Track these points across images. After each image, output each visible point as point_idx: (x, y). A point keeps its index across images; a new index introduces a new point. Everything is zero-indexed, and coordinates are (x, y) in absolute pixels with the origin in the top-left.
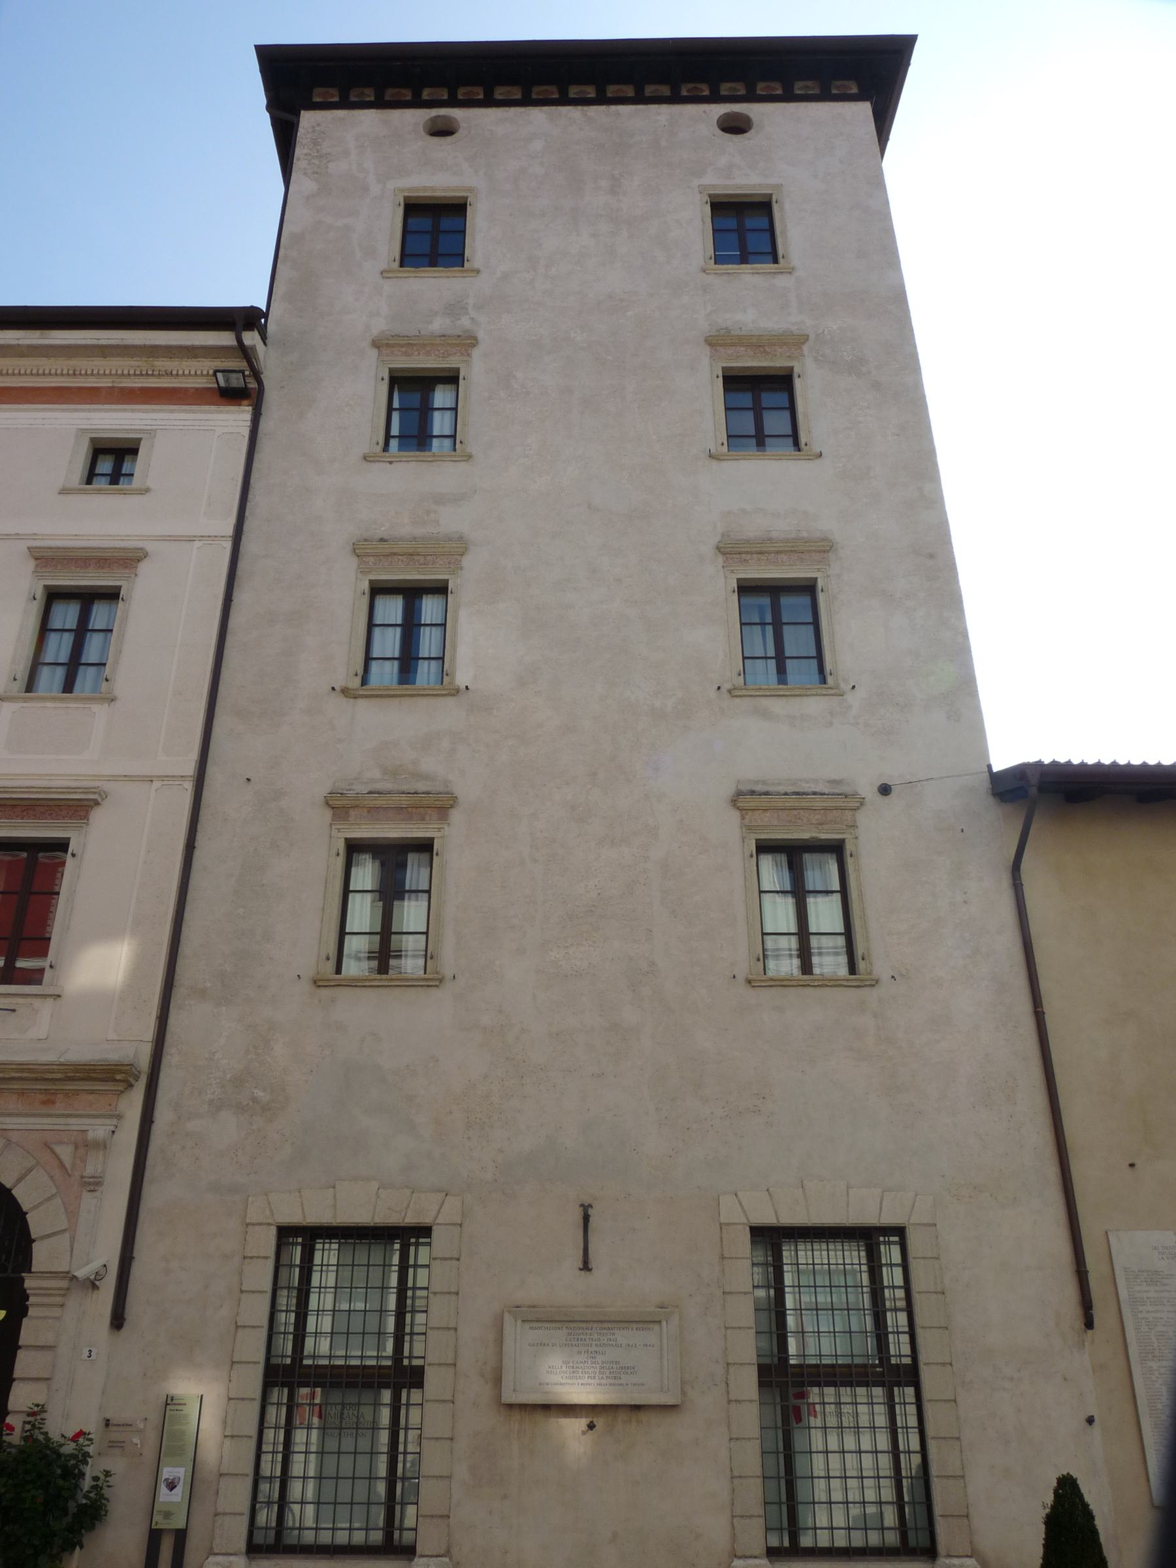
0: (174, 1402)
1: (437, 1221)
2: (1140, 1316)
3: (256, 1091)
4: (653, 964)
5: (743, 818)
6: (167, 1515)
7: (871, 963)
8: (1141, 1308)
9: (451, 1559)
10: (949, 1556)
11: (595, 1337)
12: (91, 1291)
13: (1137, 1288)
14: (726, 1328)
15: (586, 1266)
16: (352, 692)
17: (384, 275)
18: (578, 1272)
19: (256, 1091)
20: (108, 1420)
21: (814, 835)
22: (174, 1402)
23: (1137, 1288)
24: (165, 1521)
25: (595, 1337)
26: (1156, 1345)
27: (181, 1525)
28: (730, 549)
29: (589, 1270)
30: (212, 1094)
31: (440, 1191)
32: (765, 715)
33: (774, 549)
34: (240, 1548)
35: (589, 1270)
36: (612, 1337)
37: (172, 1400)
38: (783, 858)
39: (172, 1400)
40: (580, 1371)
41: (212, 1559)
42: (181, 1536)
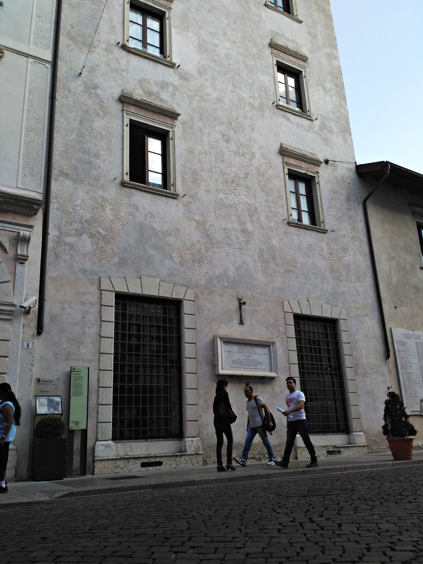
0: (75, 370)
1: (185, 298)
2: (400, 355)
3: (99, 229)
4: (256, 208)
5: (283, 159)
6: (77, 423)
7: (325, 225)
8: (401, 353)
9: (199, 438)
10: (356, 432)
11: (248, 350)
12: (23, 315)
13: (399, 346)
14: (98, 405)
15: (241, 323)
16: (128, 48)
17: (149, 215)
18: (239, 325)
19: (99, 229)
20: (39, 379)
21: (306, 172)
22: (75, 370)
23: (399, 346)
24: (75, 426)
25: (248, 350)
26: (404, 364)
27: (84, 427)
28: (274, 47)
29: (243, 324)
30: (76, 226)
31: (185, 286)
32: (288, 120)
33: (289, 53)
34: (242, 300)
35: (243, 324)
36: (254, 351)
37: (74, 369)
38: (292, 183)
39: (74, 369)
40: (244, 363)
41: (98, 443)
42: (84, 432)
